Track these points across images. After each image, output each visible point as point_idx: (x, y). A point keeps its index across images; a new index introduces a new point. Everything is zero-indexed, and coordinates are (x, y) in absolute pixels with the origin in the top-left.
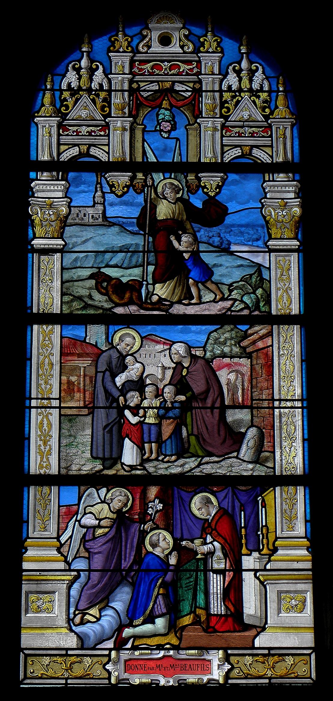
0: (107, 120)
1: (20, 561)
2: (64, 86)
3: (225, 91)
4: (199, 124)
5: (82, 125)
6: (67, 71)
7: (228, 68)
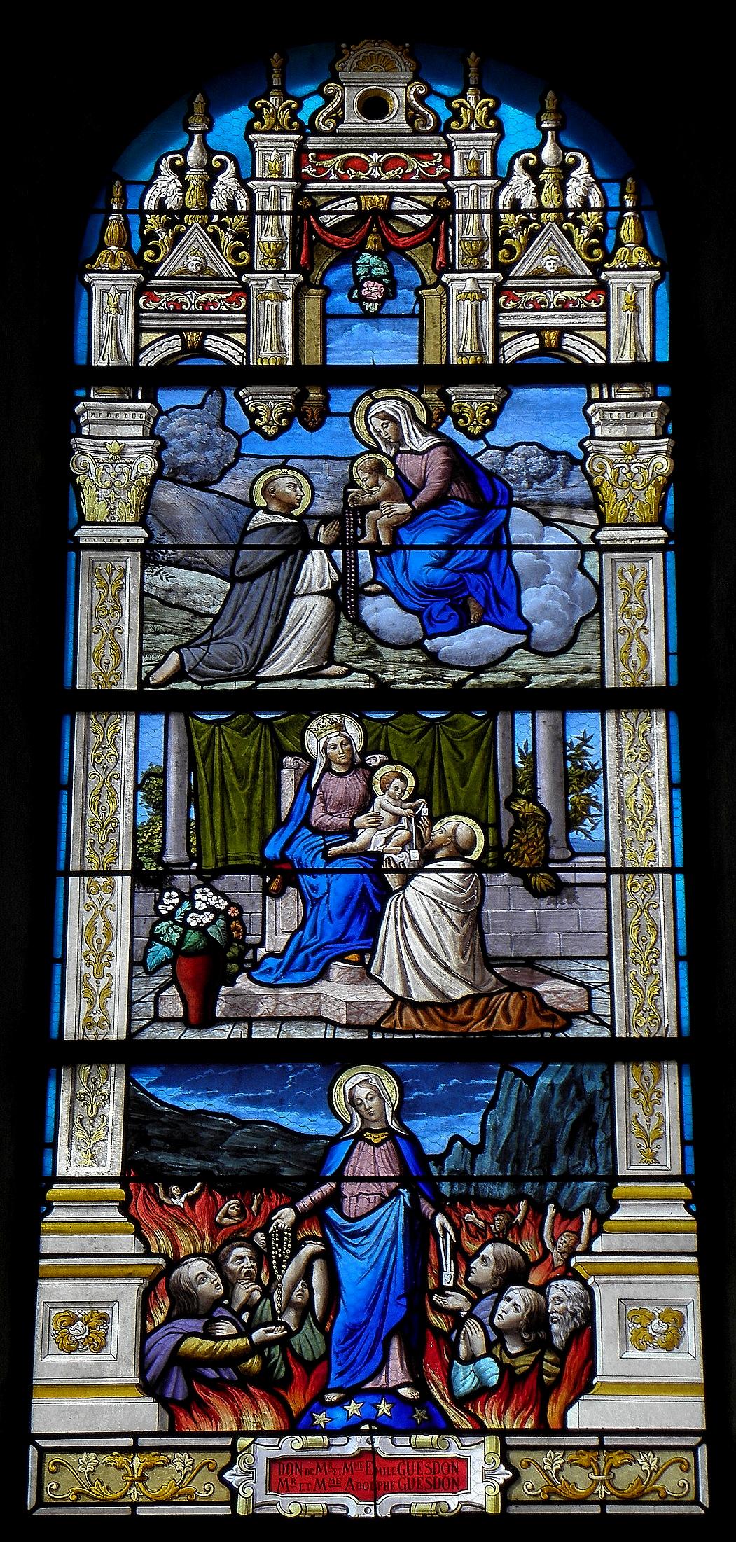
0: (243, 279)
1: (36, 1233)
2: (150, 203)
3: (504, 211)
4: (445, 286)
5: (187, 289)
6: (157, 172)
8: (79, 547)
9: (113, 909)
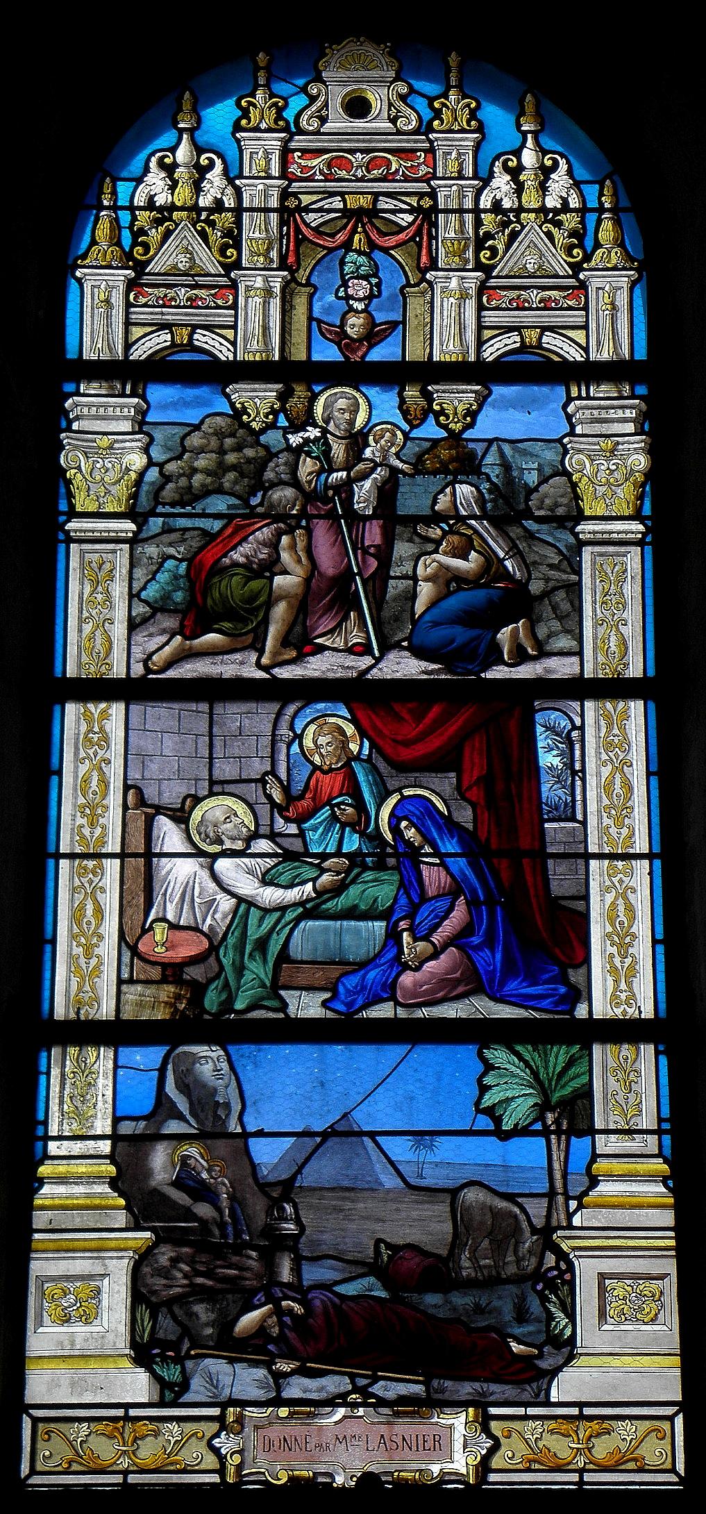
0: (232, 275)
1: (29, 1208)
2: (140, 200)
3: (140, 208)
5: (176, 285)
6: (147, 170)
7: (492, 165)
8: (69, 540)
9: (634, 891)
